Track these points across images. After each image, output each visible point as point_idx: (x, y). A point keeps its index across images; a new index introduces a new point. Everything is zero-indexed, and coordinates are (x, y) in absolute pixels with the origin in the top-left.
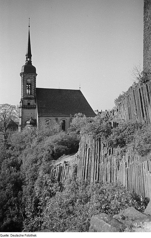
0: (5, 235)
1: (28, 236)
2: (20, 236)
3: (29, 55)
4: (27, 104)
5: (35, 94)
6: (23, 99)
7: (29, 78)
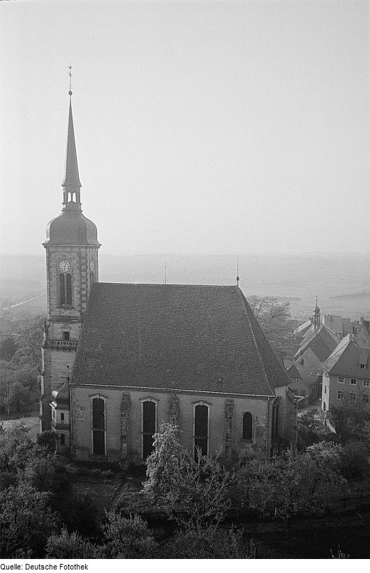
0: (12, 566)
1: (68, 567)
2: (47, 567)
3: (72, 183)
4: (61, 336)
5: (84, 305)
6: (50, 320)
7: (64, 259)
